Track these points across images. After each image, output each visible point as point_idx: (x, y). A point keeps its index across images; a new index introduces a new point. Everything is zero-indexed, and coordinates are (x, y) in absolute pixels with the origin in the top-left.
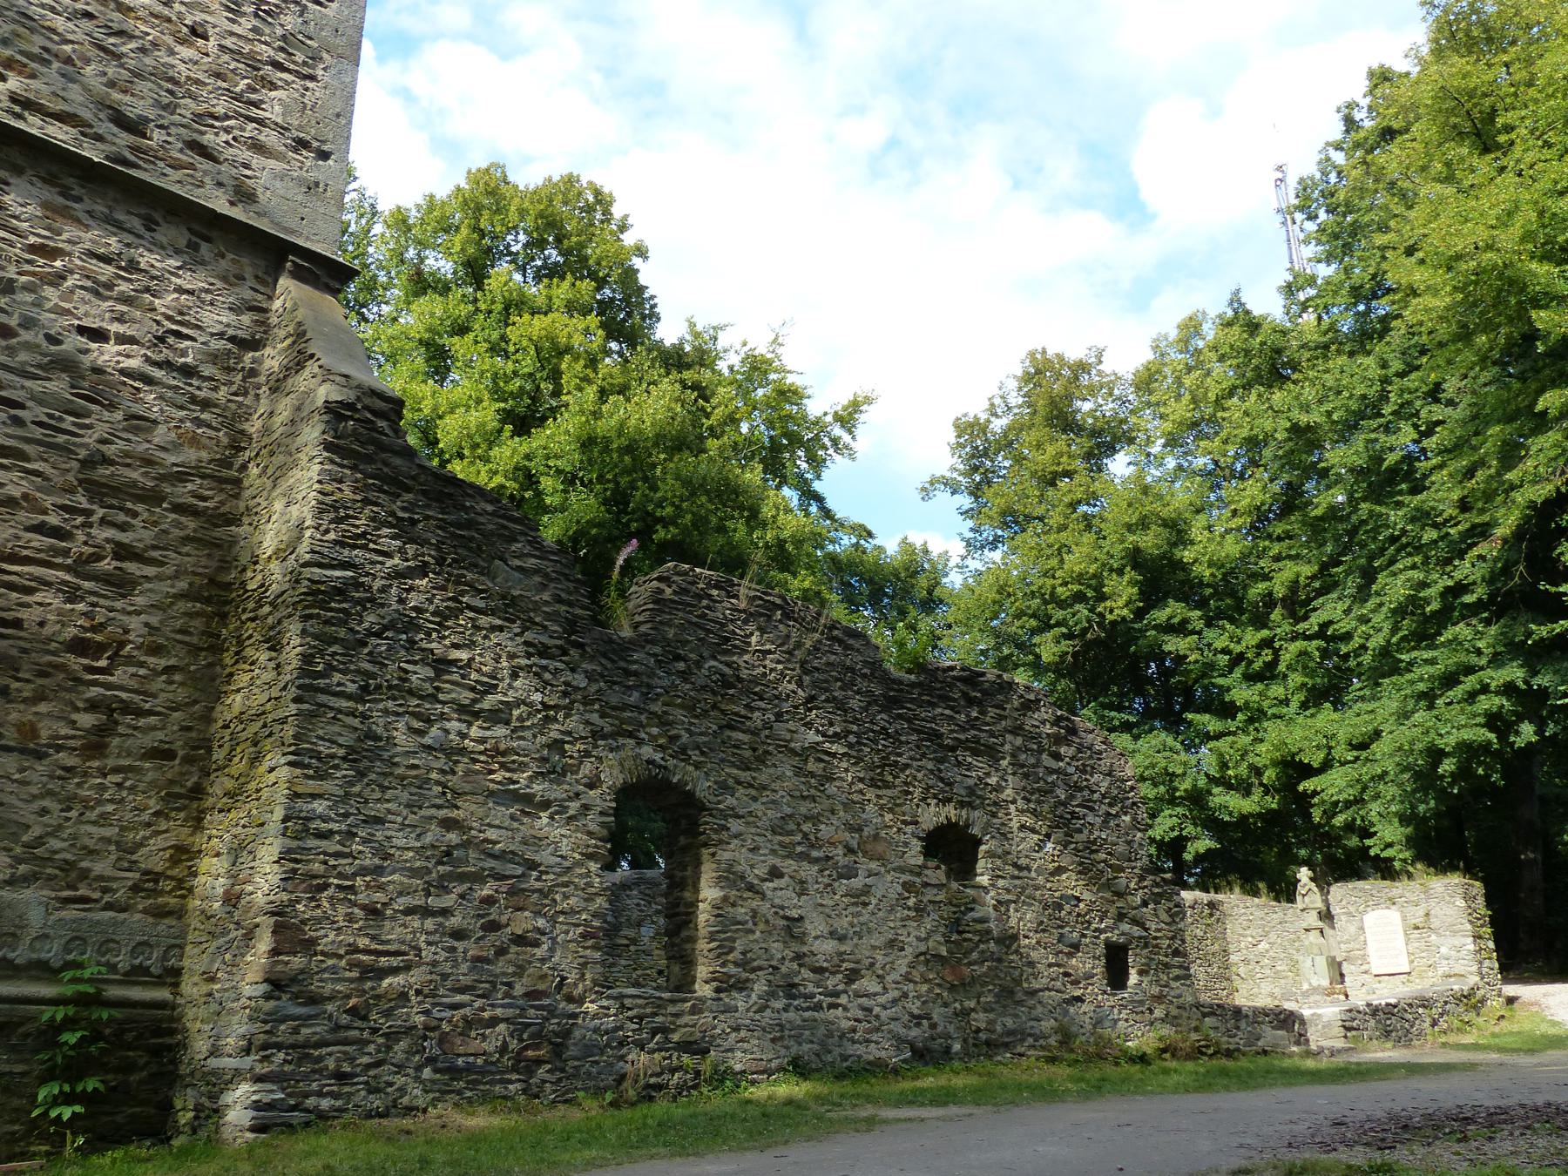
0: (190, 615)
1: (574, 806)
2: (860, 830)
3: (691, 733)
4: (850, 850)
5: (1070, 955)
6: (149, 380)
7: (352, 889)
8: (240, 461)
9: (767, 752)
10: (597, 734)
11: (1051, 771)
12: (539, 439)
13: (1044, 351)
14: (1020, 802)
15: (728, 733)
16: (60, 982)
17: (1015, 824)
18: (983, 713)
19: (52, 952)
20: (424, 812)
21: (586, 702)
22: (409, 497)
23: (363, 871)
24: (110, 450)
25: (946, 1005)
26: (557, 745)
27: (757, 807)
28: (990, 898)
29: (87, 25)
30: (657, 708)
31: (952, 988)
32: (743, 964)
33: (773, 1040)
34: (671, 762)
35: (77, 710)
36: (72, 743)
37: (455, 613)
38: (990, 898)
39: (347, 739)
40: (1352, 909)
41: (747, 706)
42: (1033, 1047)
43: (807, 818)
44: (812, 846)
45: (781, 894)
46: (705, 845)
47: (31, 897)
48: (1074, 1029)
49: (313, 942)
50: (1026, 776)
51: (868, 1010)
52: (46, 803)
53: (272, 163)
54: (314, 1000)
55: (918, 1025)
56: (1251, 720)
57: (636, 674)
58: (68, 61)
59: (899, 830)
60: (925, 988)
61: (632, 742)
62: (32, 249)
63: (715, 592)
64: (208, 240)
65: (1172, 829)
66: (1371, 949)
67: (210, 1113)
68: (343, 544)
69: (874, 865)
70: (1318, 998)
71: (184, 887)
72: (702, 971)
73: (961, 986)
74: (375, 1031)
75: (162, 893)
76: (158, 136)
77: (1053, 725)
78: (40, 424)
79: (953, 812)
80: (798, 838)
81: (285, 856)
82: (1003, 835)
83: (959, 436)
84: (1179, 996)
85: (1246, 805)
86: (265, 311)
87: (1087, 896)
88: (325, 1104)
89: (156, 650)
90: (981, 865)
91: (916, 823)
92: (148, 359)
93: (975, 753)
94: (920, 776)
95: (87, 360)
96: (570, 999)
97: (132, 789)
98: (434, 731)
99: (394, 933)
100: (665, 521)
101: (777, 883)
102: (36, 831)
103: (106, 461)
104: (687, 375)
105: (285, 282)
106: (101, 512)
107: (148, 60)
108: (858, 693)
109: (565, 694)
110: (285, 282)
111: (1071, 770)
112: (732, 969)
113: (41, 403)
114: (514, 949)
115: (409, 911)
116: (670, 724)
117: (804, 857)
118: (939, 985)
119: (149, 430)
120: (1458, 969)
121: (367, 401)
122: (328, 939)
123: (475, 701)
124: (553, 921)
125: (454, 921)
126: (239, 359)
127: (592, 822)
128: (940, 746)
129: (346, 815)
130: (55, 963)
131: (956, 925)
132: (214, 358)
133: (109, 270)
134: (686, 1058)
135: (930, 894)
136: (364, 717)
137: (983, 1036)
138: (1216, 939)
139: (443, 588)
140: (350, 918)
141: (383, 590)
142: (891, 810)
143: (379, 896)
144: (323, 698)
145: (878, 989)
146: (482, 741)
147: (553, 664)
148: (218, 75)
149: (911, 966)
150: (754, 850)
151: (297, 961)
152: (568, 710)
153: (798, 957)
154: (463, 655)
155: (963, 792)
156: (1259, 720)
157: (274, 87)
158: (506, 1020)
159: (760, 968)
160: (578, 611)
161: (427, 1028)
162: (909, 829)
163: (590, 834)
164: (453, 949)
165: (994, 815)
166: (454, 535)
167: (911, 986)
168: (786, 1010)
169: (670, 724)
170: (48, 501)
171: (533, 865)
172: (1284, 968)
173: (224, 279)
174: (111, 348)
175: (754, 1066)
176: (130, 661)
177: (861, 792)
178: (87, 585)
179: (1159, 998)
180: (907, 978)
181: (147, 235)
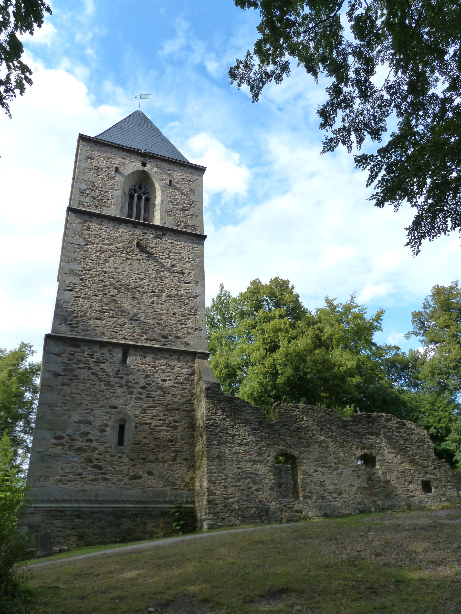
0: (188, 431)
1: (265, 461)
2: (338, 458)
3: (291, 442)
4: (336, 464)
5: (409, 485)
6: (175, 387)
7: (221, 483)
8: (193, 399)
9: (311, 443)
10: (269, 445)
11: (397, 436)
12: (275, 355)
13: (438, 286)
14: (388, 446)
15: (300, 440)
16: (174, 504)
17: (386, 452)
18: (373, 424)
19: (172, 499)
20: (233, 466)
21: (265, 438)
22: (223, 403)
23: (223, 479)
24: (170, 402)
25: (368, 499)
26: (260, 449)
27: (310, 456)
28: (380, 472)
29: (155, 320)
30: (282, 437)
31: (370, 495)
32: (310, 492)
33: (319, 509)
34: (287, 449)
35: (171, 453)
36: (171, 459)
37: (235, 425)
38: (380, 472)
39: (217, 454)
41: (305, 433)
42: (398, 509)
43: (323, 457)
44: (325, 464)
45: (317, 475)
46: (298, 466)
47: (168, 488)
48: (412, 504)
49: (215, 493)
50: (389, 439)
51: (346, 502)
52: (168, 471)
53: (191, 335)
54: (216, 504)
55: (360, 505)
57: (276, 430)
58: (153, 328)
59: (350, 457)
60: (361, 495)
61: (277, 446)
62: (152, 367)
63: (294, 409)
64: (181, 355)
67: (202, 527)
68: (211, 415)
69: (343, 467)
71: (193, 485)
72: (301, 495)
73: (374, 494)
74: (228, 510)
75: (190, 486)
76: (170, 337)
77: (397, 424)
78: (158, 400)
79: (366, 451)
80: (321, 462)
81: (208, 478)
82: (383, 455)
83: (414, 318)
84: (450, 494)
86: (194, 367)
87: (413, 468)
88: (221, 524)
89: (183, 439)
90: (377, 463)
91: (355, 455)
92: (174, 383)
93: (371, 435)
94: (355, 443)
95: (164, 386)
96: (268, 502)
97: (182, 467)
98: (234, 449)
99: (230, 491)
100: (309, 373)
101: (316, 473)
102: (167, 477)
103: (169, 404)
104: (315, 326)
105: (197, 360)
106: (170, 414)
107: (166, 323)
108: (335, 425)
109: (261, 438)
110: (197, 360)
111: (404, 435)
112: (307, 494)
113: (158, 396)
114: (255, 492)
115: (233, 486)
116: (286, 440)
117: (323, 466)
118: (366, 495)
119: (176, 397)
121: (213, 385)
122: (218, 493)
123: (241, 442)
124: (263, 486)
125: (242, 487)
126: (190, 378)
127: (269, 464)
128: (360, 435)
129: (218, 468)
130: (173, 501)
131: (370, 479)
132: (186, 379)
133: (165, 367)
134: (297, 514)
135: (360, 473)
136: (219, 449)
137: (381, 507)
139: (232, 420)
140: (221, 488)
141: (220, 423)
142: (347, 453)
143: (226, 484)
144: (211, 446)
145: (348, 496)
146: (244, 450)
147: (257, 432)
148: (179, 321)
149: (357, 490)
150: (310, 466)
151: (212, 497)
152: (262, 441)
153: (324, 490)
154: (238, 433)
155: (368, 445)
157: (189, 319)
158: (255, 507)
159: (314, 493)
160: (262, 419)
161: (239, 509)
162: (353, 457)
163: (269, 467)
164: (242, 493)
165: (379, 450)
166: (233, 409)
167: (357, 495)
168: (322, 502)
169: (286, 440)
170: (161, 414)
171: (257, 475)
173: (185, 362)
174: (167, 382)
175: (314, 515)
176: (179, 442)
177: (338, 449)
178: (169, 429)
179: (443, 495)
180: (356, 493)
181: (171, 358)
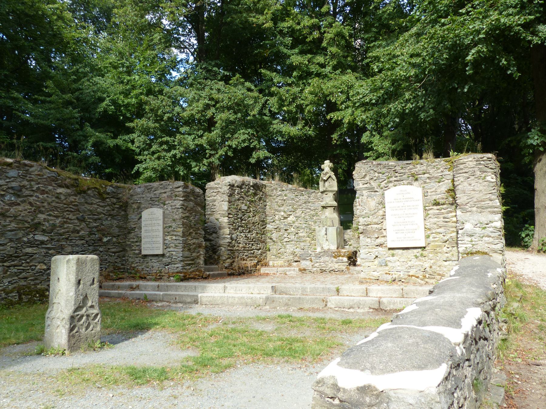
40: (374, 184)
56: (300, 78)
65: (244, 141)
66: (389, 223)
70: (327, 259)
85: (294, 130)
120: (481, 246)
138: (258, 212)
156: (306, 78)
172: (304, 234)
